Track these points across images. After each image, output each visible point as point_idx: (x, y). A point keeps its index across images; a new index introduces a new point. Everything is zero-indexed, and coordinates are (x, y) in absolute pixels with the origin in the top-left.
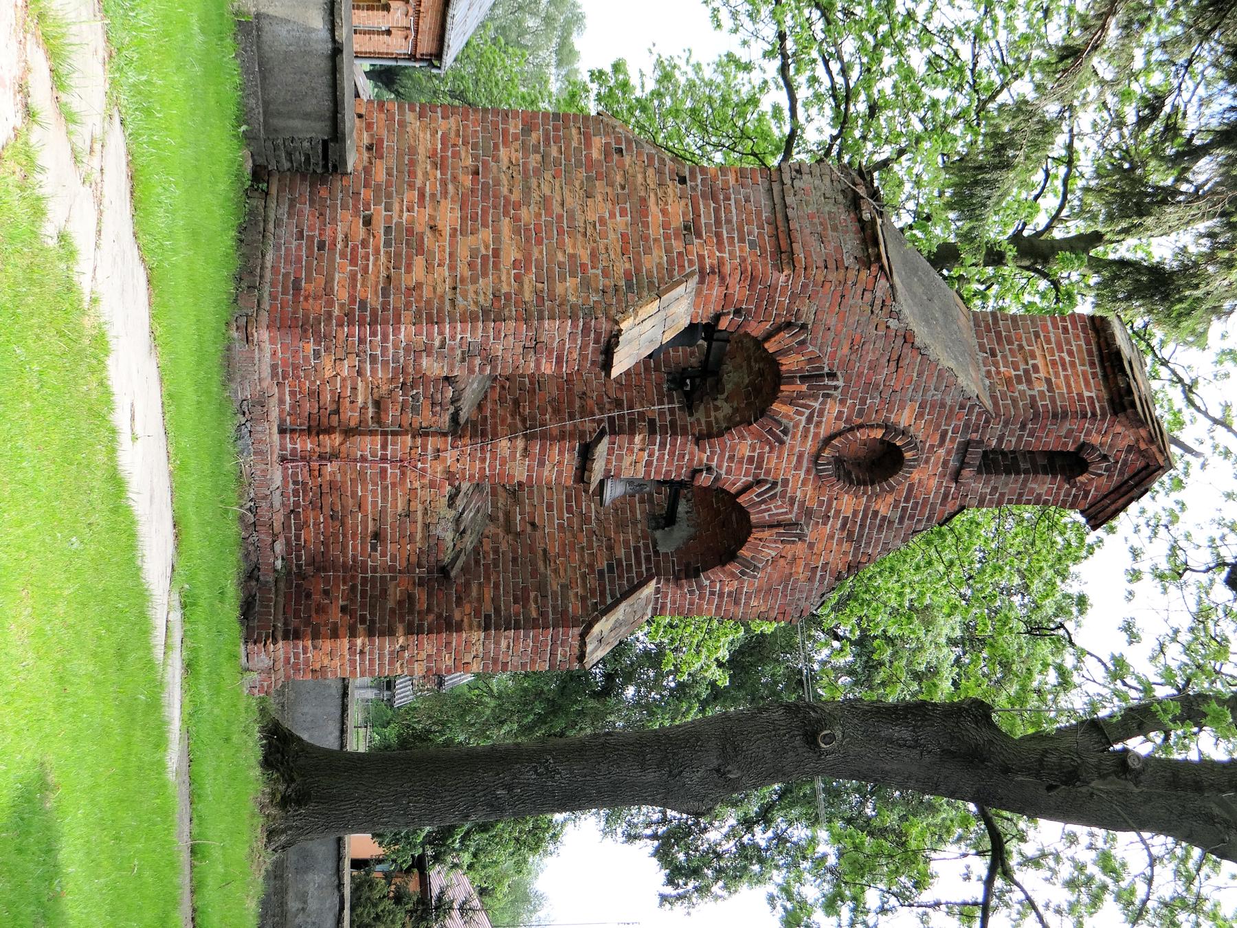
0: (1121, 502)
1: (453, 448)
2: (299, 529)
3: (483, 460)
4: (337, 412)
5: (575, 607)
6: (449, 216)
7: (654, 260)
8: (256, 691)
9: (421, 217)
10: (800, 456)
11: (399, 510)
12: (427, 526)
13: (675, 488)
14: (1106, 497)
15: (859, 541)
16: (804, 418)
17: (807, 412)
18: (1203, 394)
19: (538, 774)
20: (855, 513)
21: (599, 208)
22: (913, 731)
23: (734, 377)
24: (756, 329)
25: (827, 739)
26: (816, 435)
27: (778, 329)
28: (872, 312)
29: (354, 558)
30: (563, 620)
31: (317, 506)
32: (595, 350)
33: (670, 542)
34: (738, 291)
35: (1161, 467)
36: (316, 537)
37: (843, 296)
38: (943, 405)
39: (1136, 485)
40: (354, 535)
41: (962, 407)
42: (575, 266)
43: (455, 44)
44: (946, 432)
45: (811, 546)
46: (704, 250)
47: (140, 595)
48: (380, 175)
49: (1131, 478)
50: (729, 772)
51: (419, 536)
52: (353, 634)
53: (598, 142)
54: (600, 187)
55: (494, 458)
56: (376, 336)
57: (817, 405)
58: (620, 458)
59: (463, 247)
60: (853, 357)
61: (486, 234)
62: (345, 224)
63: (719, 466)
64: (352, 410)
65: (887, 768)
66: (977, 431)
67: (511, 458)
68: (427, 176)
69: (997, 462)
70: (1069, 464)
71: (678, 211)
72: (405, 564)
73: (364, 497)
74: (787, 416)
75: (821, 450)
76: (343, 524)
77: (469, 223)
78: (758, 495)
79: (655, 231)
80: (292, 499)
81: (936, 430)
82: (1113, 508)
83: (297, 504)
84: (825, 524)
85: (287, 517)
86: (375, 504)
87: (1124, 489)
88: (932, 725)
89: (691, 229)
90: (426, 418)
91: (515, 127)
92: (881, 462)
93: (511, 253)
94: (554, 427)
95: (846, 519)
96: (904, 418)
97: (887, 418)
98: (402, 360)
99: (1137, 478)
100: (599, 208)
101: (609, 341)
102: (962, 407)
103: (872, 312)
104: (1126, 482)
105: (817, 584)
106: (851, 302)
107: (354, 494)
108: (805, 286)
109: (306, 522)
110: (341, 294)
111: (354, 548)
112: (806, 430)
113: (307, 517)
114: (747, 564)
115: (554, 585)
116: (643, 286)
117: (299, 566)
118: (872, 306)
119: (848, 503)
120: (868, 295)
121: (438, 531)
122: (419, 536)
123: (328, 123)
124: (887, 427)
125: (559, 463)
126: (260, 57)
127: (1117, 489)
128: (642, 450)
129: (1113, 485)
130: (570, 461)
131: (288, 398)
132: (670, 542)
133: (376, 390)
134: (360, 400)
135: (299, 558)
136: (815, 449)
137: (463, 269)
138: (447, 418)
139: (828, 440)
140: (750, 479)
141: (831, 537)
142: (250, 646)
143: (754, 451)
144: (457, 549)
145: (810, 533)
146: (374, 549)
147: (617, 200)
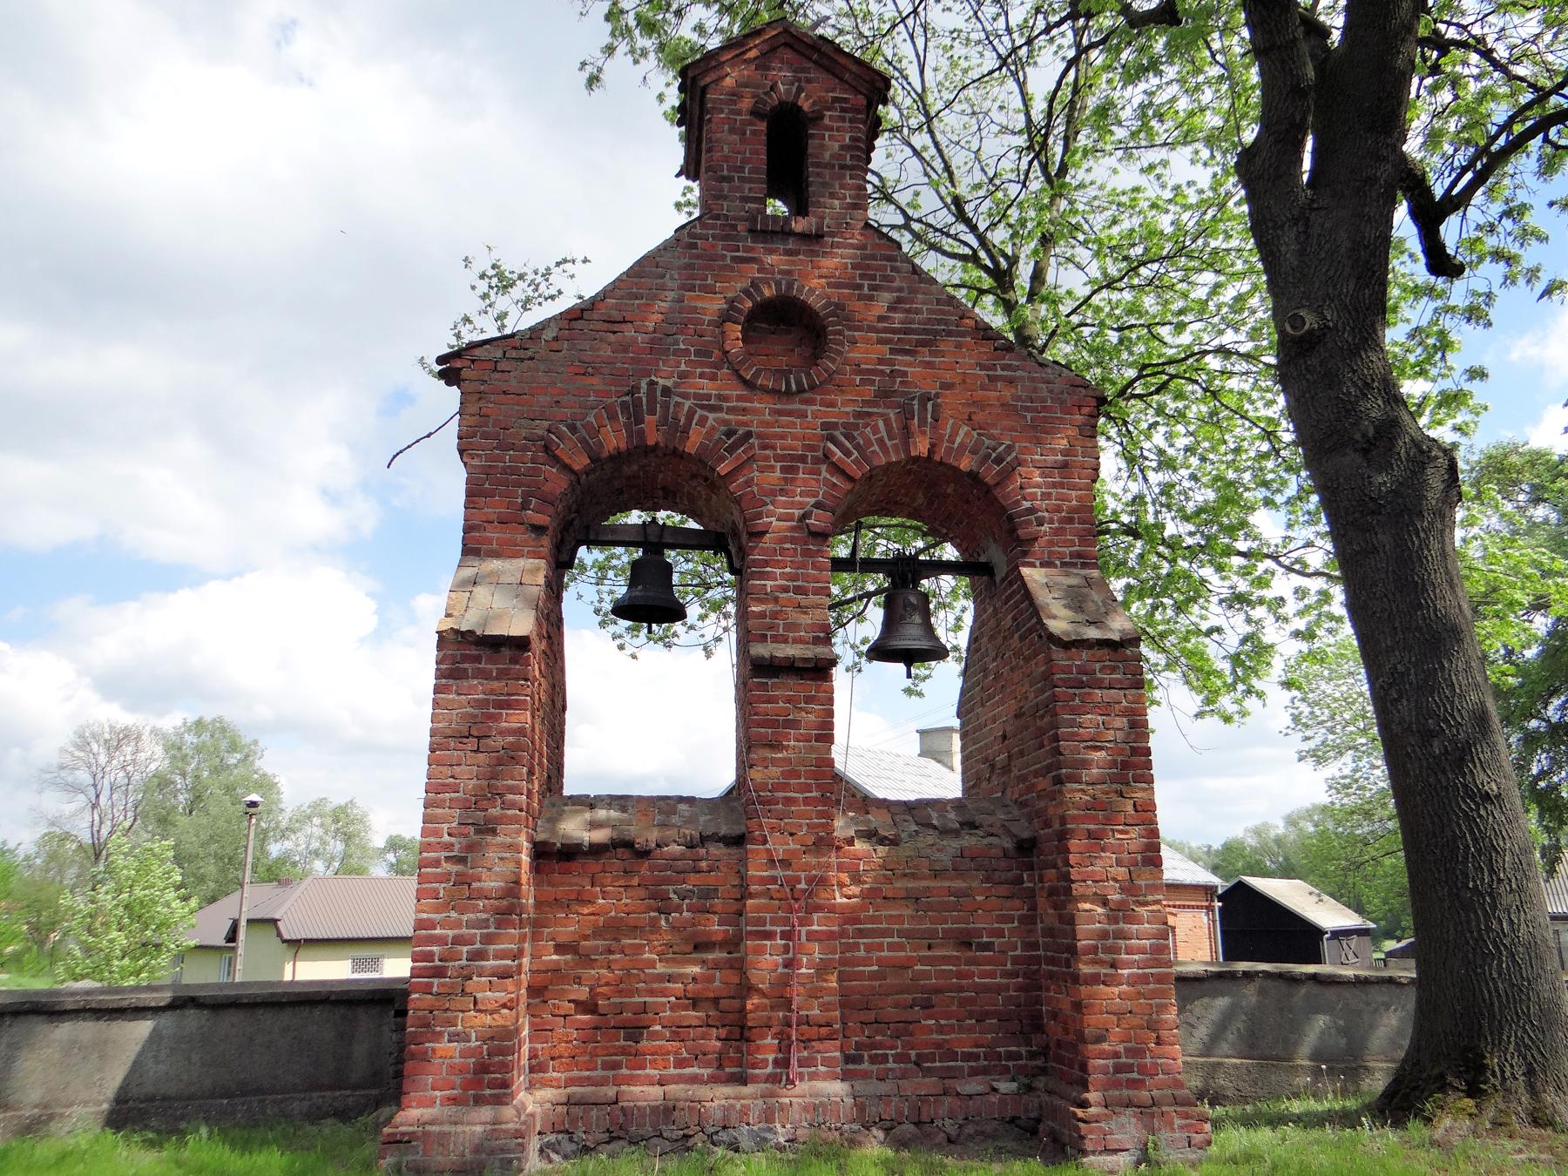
0: (842, 60)
2: (953, 1056)
4: (716, 1001)
8: (1197, 1138)
10: (780, 413)
11: (909, 912)
12: (936, 874)
15: (936, 332)
16: (711, 416)
17: (699, 412)
19: (1401, 697)
20: (881, 341)
22: (1282, 227)
25: (1298, 323)
26: (740, 398)
27: (556, 460)
28: (531, 359)
29: (1006, 974)
31: (904, 1029)
35: (786, 31)
36: (970, 1029)
38: (690, 266)
39: (819, 51)
40: (960, 975)
41: (693, 246)
44: (733, 258)
45: (947, 386)
49: (810, 59)
50: (1364, 435)
51: (959, 884)
52: (1076, 979)
55: (785, 787)
56: (432, 954)
57: (687, 404)
60: (606, 371)
63: (801, 505)
64: (711, 979)
65: (1347, 244)
66: (734, 227)
72: (1017, 902)
73: (880, 962)
74: (709, 435)
76: (938, 991)
78: (847, 453)
80: (891, 1065)
82: (854, 68)
83: (899, 1058)
84: (905, 374)
85: (928, 1072)
86: (892, 947)
87: (825, 61)
90: (724, 881)
92: (786, 321)
95: (892, 351)
97: (710, 323)
98: (484, 916)
102: (693, 246)
103: (531, 359)
104: (816, 62)
105: (1019, 373)
106: (514, 382)
107: (873, 976)
108: (485, 436)
109: (938, 1045)
111: (992, 975)
112: (731, 410)
113: (927, 1044)
117: (1032, 1055)
118: (522, 360)
121: (945, 859)
122: (959, 884)
123: (360, 1010)
126: (228, 1094)
127: (828, 70)
129: (823, 76)
131: (688, 1071)
133: (676, 948)
134: (696, 969)
135: (1011, 1056)
136: (766, 397)
140: (824, 467)
141: (929, 365)
142: (1089, 1146)
143: (773, 467)
144: (1000, 832)
146: (988, 947)
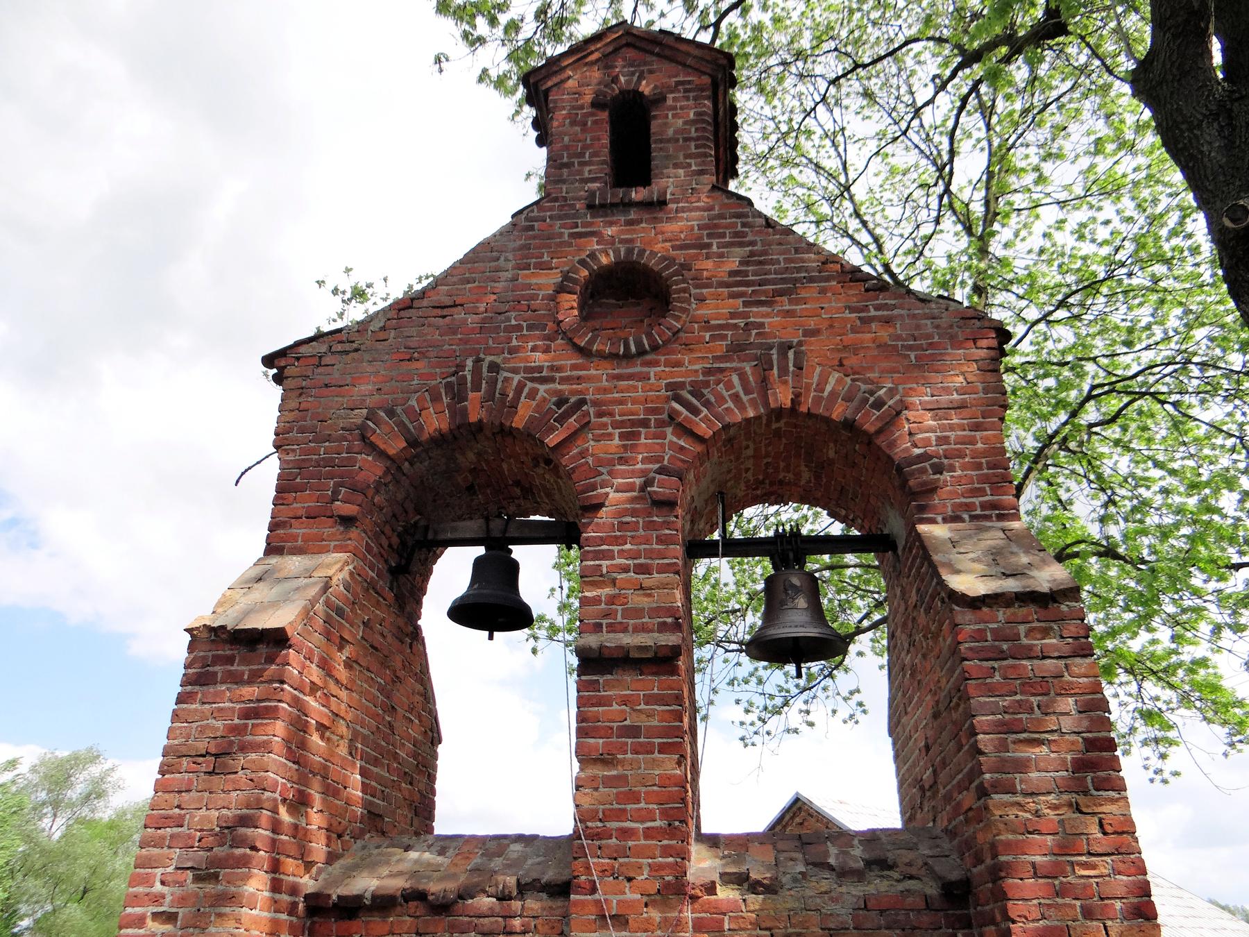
1: (593, 890)
3: (625, 833)
14: (684, 65)
18: (1014, 215)
22: (1199, 126)
32: (244, 661)
37: (326, 386)
39: (660, 44)
49: (652, 53)
58: (637, 612)
75: (602, 355)
81: (570, 245)
87: (667, 52)
88: (1179, 110)
99: (649, 47)
101: (225, 641)
104: (658, 55)
120: (327, 360)
128: (614, 582)
139: (584, 352)
140: (669, 430)
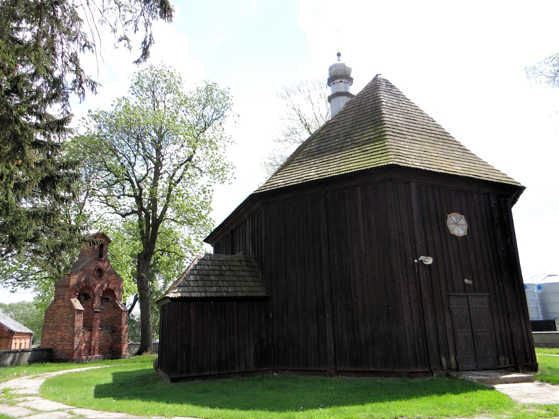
5: (119, 312)
6: (59, 333)
7: (67, 304)
9: (59, 337)
13: (102, 299)
21: (59, 312)
23: (86, 291)
24: (79, 290)
30: (121, 314)
31: (102, 349)
33: (111, 298)
34: (73, 293)
42: (67, 315)
43: (29, 331)
46: (66, 297)
47: (101, 369)
48: (52, 343)
53: (49, 312)
54: (56, 312)
59: (63, 331)
61: (62, 328)
62: (59, 348)
67: (97, 323)
68: (53, 336)
69: (101, 256)
70: (102, 246)
71: (61, 301)
77: (61, 331)
79: (63, 304)
89: (63, 299)
91: (46, 324)
92: (100, 271)
93: (65, 324)
94: (92, 317)
96: (93, 268)
100: (59, 312)
110: (69, 348)
114: (114, 289)
115: (116, 315)
116: (71, 306)
119: (106, 275)
124: (95, 270)
125: (97, 316)
130: (97, 314)
132: (111, 298)
137: (67, 331)
138: (188, 171)
145: (110, 280)
147: (58, 309)
